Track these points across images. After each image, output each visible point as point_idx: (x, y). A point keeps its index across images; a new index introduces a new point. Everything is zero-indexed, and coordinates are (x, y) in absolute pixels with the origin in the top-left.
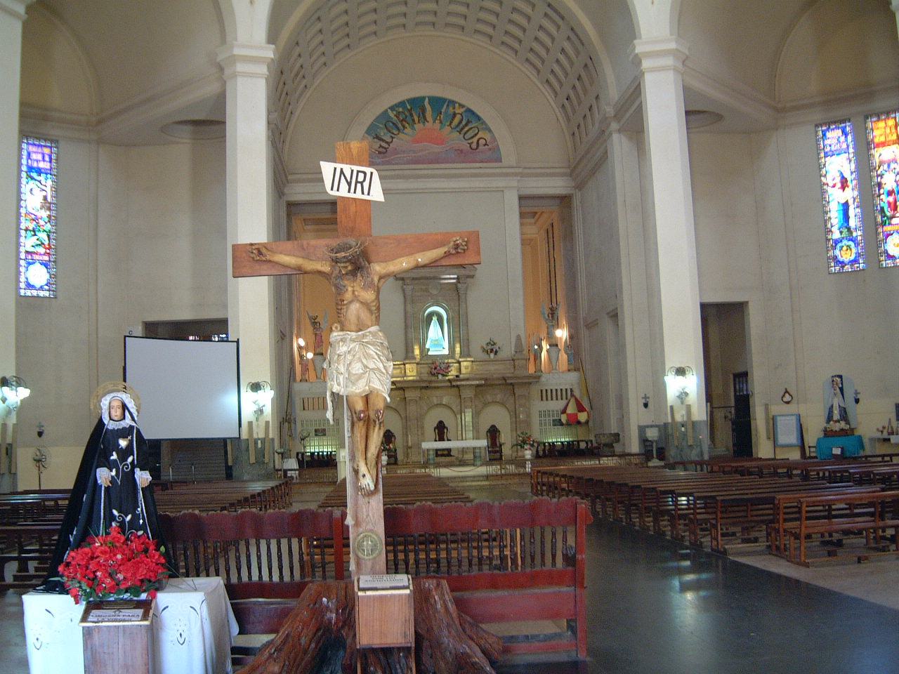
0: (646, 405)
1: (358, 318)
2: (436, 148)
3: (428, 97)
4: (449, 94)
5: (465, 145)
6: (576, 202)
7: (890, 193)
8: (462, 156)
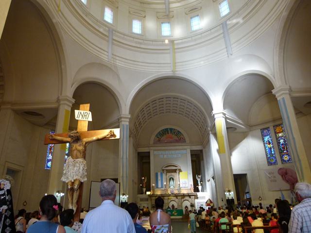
0: (222, 200)
1: (76, 155)
2: (171, 140)
3: (201, 151)
4: (173, 127)
5: (177, 139)
6: (204, 151)
7: (282, 144)
8: (177, 141)
